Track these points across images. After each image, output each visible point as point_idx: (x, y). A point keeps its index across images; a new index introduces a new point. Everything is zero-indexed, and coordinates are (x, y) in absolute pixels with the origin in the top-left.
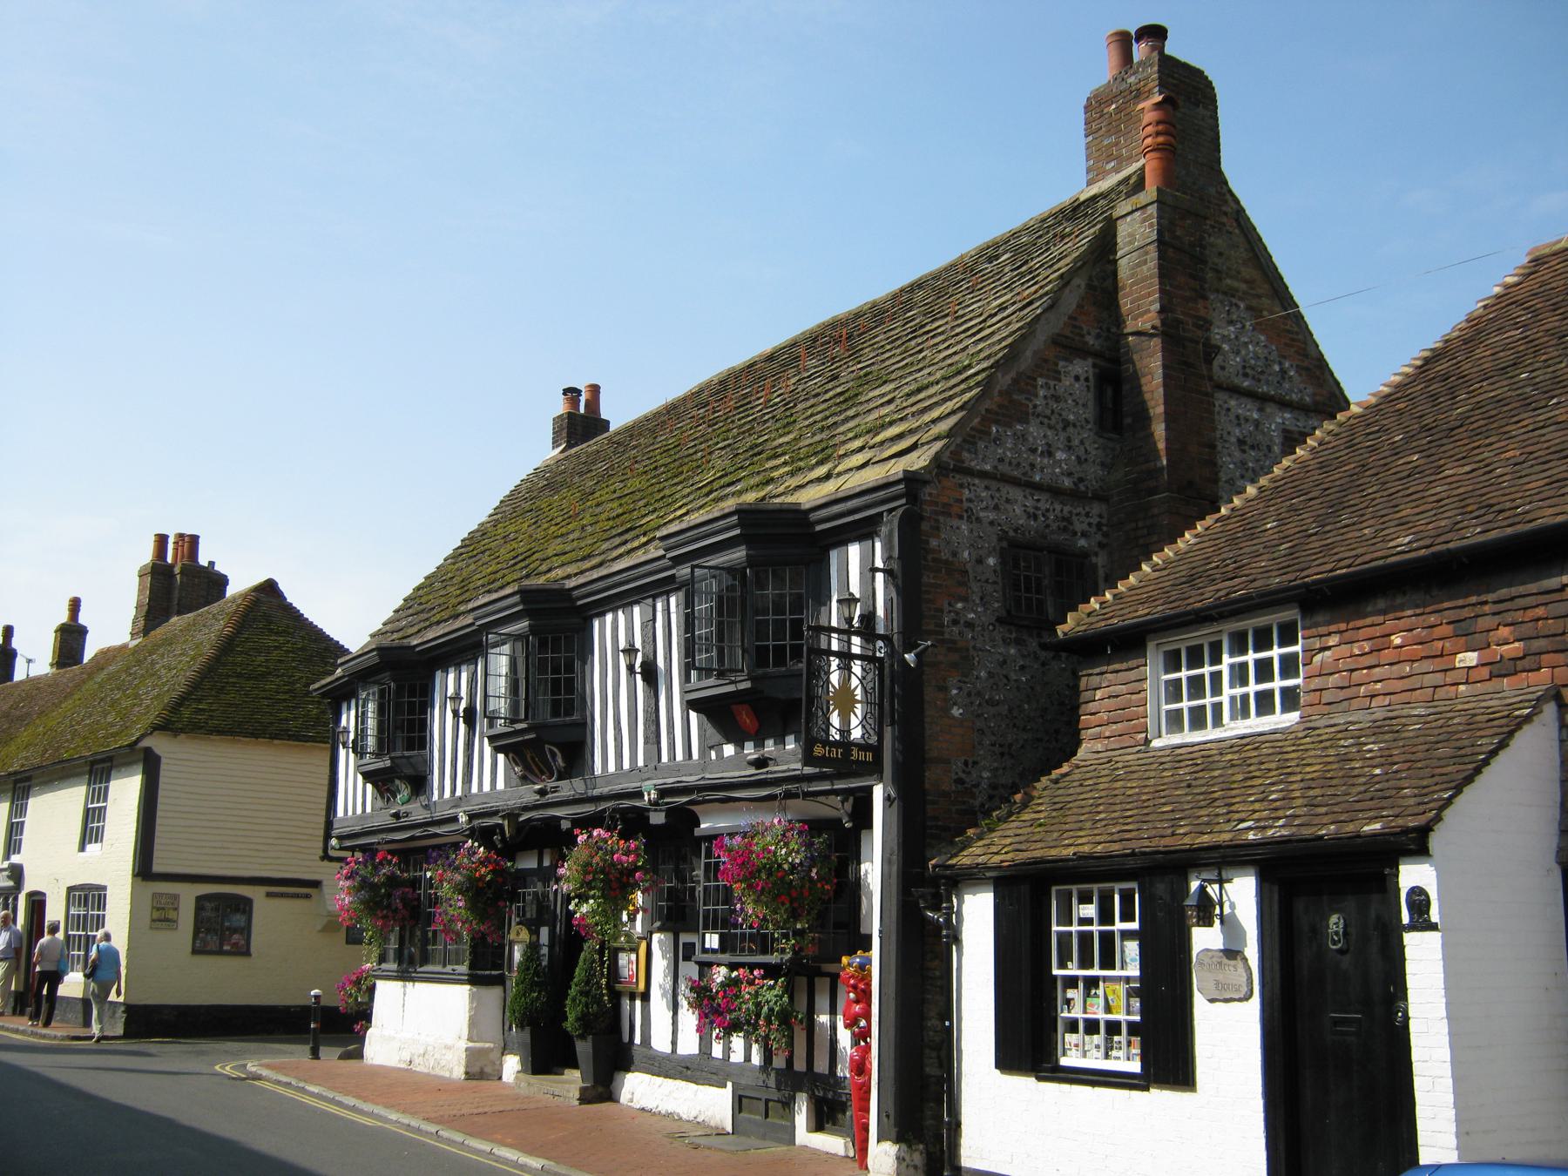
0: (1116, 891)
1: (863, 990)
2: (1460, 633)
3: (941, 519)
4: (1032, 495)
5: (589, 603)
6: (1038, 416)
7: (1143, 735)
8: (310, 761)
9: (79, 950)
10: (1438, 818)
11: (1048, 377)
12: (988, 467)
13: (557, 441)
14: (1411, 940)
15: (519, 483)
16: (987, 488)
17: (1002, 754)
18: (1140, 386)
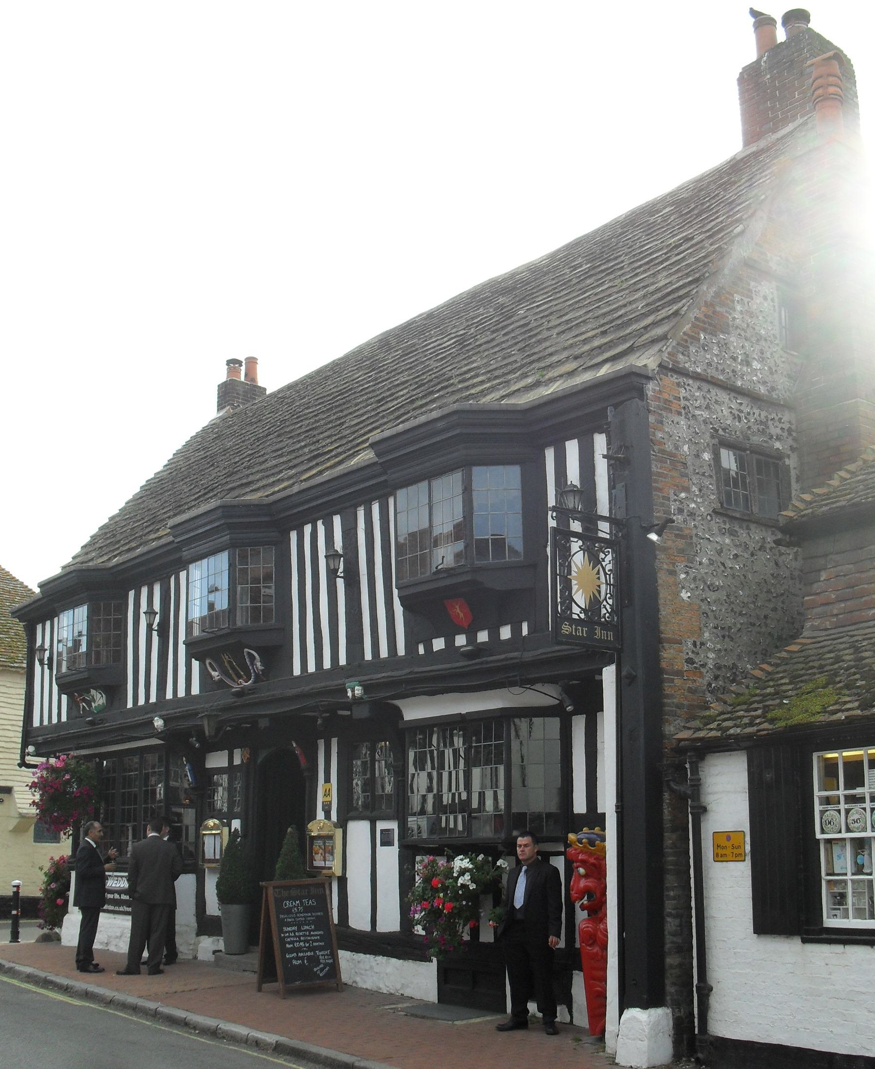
4: (736, 398)
12: (699, 370)
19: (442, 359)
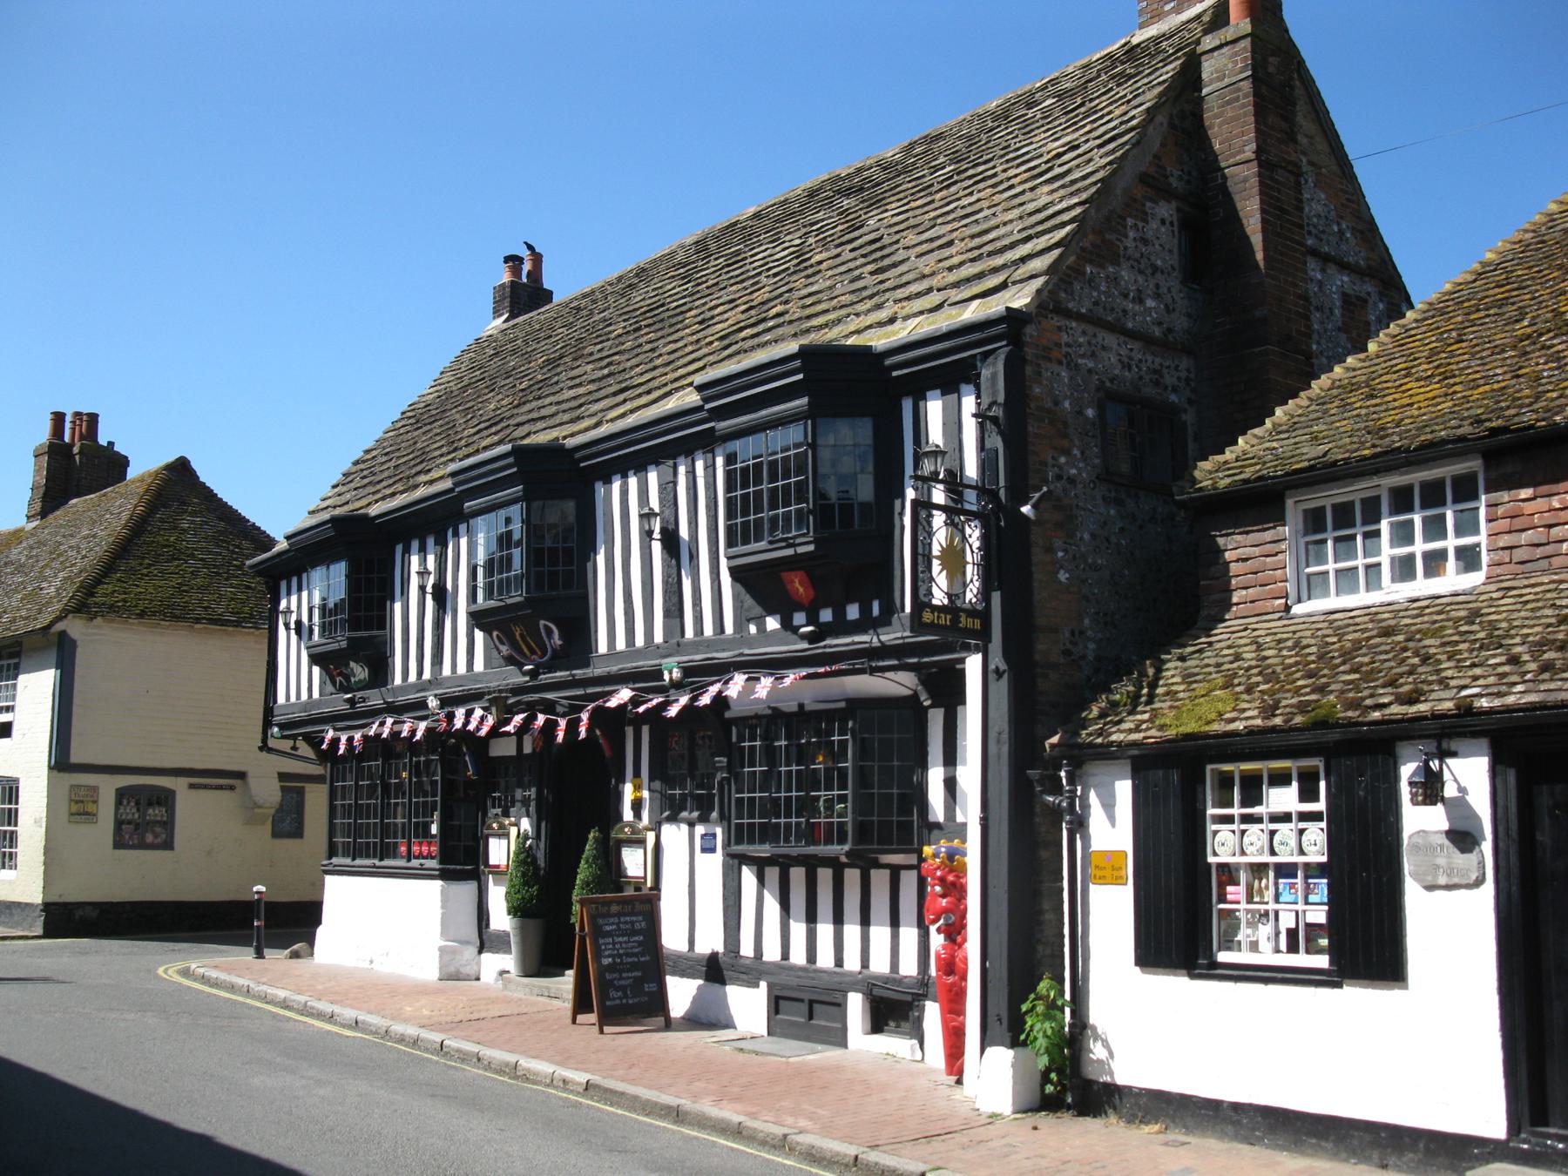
1: (953, 884)
4: (1126, 344)
6: (1129, 259)
7: (1283, 601)
8: (249, 646)
12: (1084, 311)
13: (499, 311)
15: (460, 354)
16: (1084, 333)
19: (775, 275)
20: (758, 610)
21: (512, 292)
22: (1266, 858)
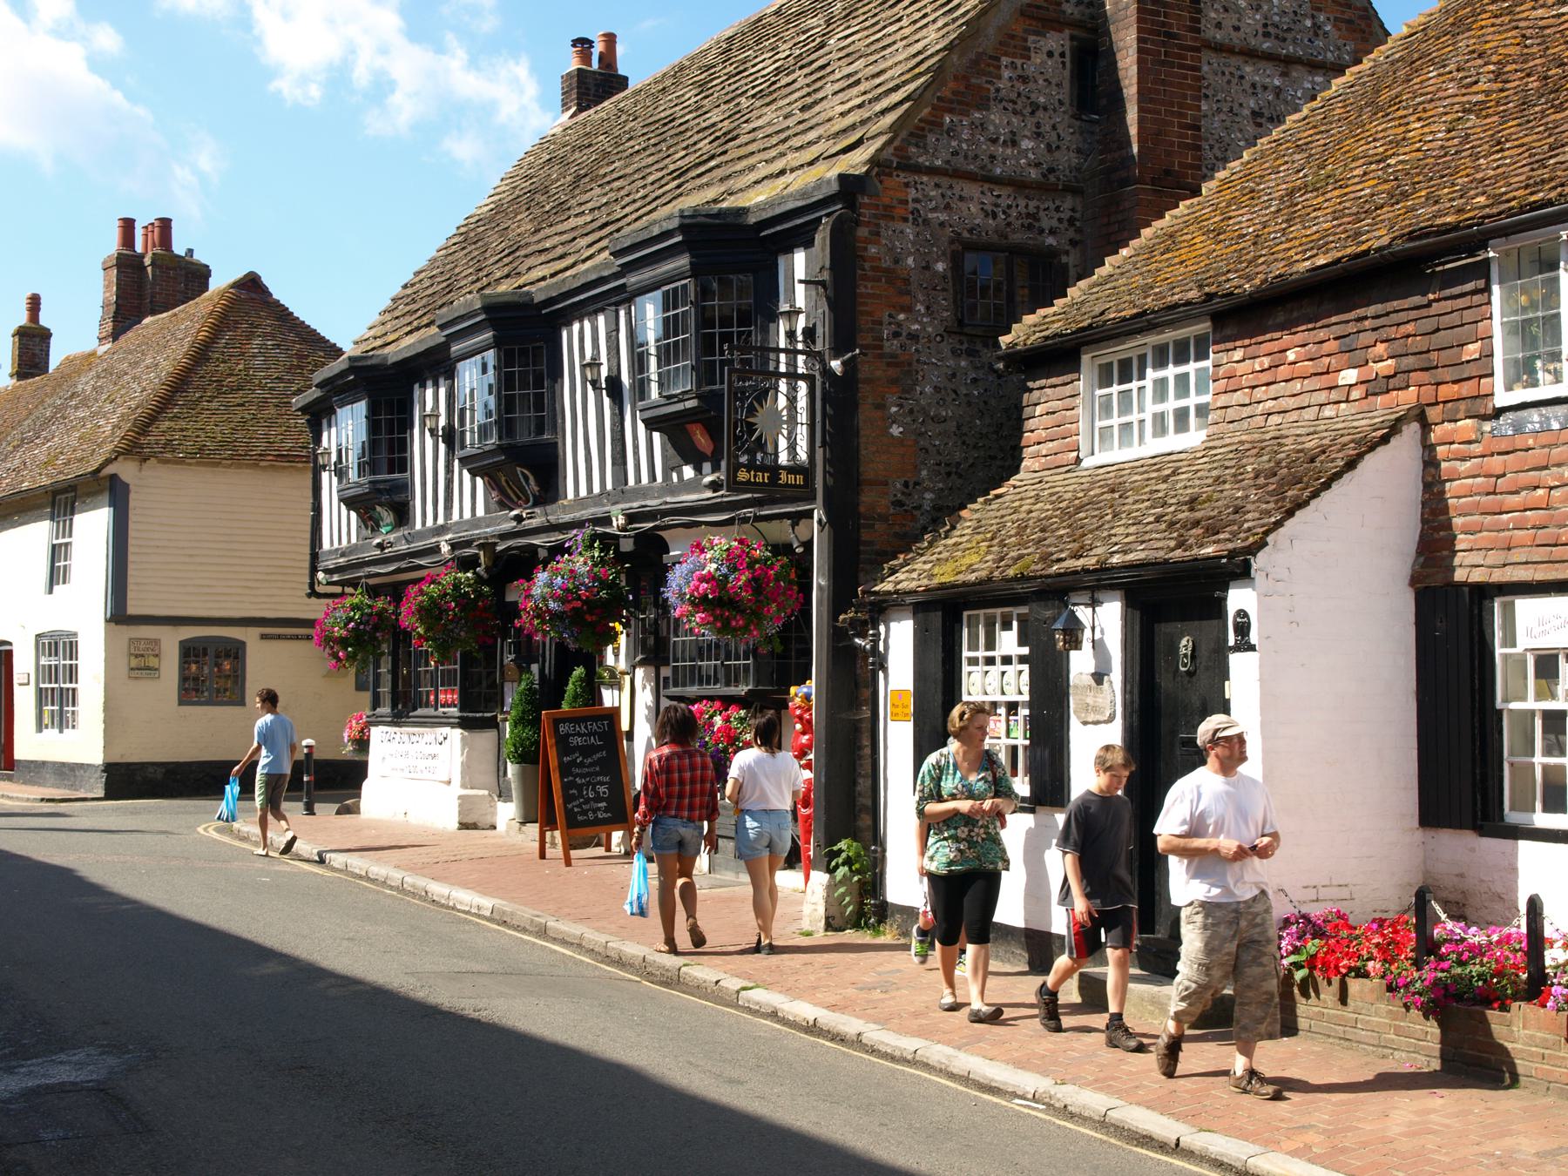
0: (1015, 617)
2: (1344, 349)
3: (882, 223)
4: (991, 191)
5: (574, 303)
7: (1075, 454)
8: (294, 485)
9: (53, 704)
10: (1261, 544)
11: (1014, 55)
12: (939, 163)
14: (1236, 661)
15: (523, 156)
16: (937, 186)
17: (949, 474)
18: (1115, 63)
20: (678, 459)
21: (579, 81)
22: (998, 698)
